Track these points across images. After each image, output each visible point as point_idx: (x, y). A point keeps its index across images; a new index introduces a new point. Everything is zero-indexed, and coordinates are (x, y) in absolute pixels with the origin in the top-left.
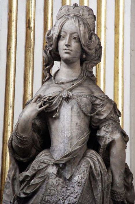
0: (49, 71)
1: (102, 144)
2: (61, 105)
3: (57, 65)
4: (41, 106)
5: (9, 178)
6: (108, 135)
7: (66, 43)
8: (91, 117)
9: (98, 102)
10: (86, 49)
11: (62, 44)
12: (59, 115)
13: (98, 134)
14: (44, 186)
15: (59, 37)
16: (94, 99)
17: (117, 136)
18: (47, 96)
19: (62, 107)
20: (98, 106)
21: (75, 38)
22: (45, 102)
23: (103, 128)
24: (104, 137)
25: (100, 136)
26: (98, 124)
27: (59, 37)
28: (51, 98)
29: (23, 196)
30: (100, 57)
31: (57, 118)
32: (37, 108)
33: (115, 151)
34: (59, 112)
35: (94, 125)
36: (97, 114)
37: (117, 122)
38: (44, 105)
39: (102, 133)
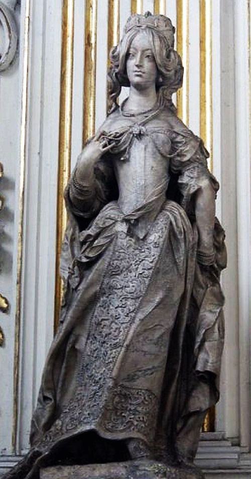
0: (115, 99)
1: (185, 193)
2: (131, 144)
3: (125, 92)
4: (105, 146)
5: (67, 238)
6: (193, 182)
7: (137, 63)
8: (171, 159)
9: (179, 139)
10: (163, 70)
11: (132, 64)
12: (129, 157)
13: (180, 181)
14: (111, 248)
15: (127, 55)
16: (174, 135)
17: (204, 183)
18: (113, 132)
19: (133, 146)
20: (180, 145)
21: (148, 56)
22: (111, 140)
23: (186, 173)
24: (187, 185)
25: (182, 184)
26: (180, 168)
27: (127, 55)
28: (118, 135)
29: (84, 260)
30: (181, 80)
31: (127, 161)
32: (101, 148)
33: (201, 202)
34: (129, 153)
35: (175, 169)
36: (178, 155)
37: (205, 165)
38: (110, 144)
39: (184, 180)
